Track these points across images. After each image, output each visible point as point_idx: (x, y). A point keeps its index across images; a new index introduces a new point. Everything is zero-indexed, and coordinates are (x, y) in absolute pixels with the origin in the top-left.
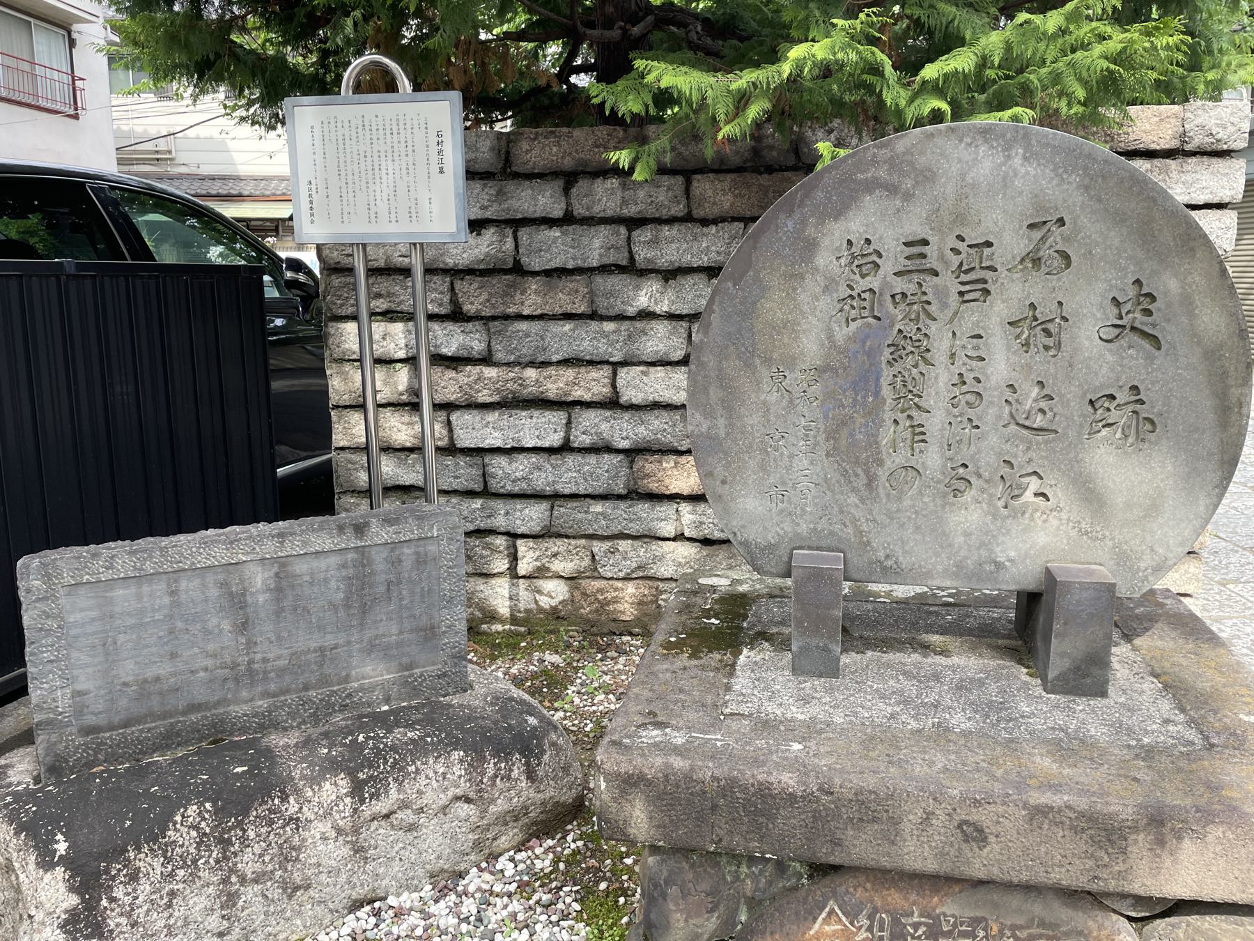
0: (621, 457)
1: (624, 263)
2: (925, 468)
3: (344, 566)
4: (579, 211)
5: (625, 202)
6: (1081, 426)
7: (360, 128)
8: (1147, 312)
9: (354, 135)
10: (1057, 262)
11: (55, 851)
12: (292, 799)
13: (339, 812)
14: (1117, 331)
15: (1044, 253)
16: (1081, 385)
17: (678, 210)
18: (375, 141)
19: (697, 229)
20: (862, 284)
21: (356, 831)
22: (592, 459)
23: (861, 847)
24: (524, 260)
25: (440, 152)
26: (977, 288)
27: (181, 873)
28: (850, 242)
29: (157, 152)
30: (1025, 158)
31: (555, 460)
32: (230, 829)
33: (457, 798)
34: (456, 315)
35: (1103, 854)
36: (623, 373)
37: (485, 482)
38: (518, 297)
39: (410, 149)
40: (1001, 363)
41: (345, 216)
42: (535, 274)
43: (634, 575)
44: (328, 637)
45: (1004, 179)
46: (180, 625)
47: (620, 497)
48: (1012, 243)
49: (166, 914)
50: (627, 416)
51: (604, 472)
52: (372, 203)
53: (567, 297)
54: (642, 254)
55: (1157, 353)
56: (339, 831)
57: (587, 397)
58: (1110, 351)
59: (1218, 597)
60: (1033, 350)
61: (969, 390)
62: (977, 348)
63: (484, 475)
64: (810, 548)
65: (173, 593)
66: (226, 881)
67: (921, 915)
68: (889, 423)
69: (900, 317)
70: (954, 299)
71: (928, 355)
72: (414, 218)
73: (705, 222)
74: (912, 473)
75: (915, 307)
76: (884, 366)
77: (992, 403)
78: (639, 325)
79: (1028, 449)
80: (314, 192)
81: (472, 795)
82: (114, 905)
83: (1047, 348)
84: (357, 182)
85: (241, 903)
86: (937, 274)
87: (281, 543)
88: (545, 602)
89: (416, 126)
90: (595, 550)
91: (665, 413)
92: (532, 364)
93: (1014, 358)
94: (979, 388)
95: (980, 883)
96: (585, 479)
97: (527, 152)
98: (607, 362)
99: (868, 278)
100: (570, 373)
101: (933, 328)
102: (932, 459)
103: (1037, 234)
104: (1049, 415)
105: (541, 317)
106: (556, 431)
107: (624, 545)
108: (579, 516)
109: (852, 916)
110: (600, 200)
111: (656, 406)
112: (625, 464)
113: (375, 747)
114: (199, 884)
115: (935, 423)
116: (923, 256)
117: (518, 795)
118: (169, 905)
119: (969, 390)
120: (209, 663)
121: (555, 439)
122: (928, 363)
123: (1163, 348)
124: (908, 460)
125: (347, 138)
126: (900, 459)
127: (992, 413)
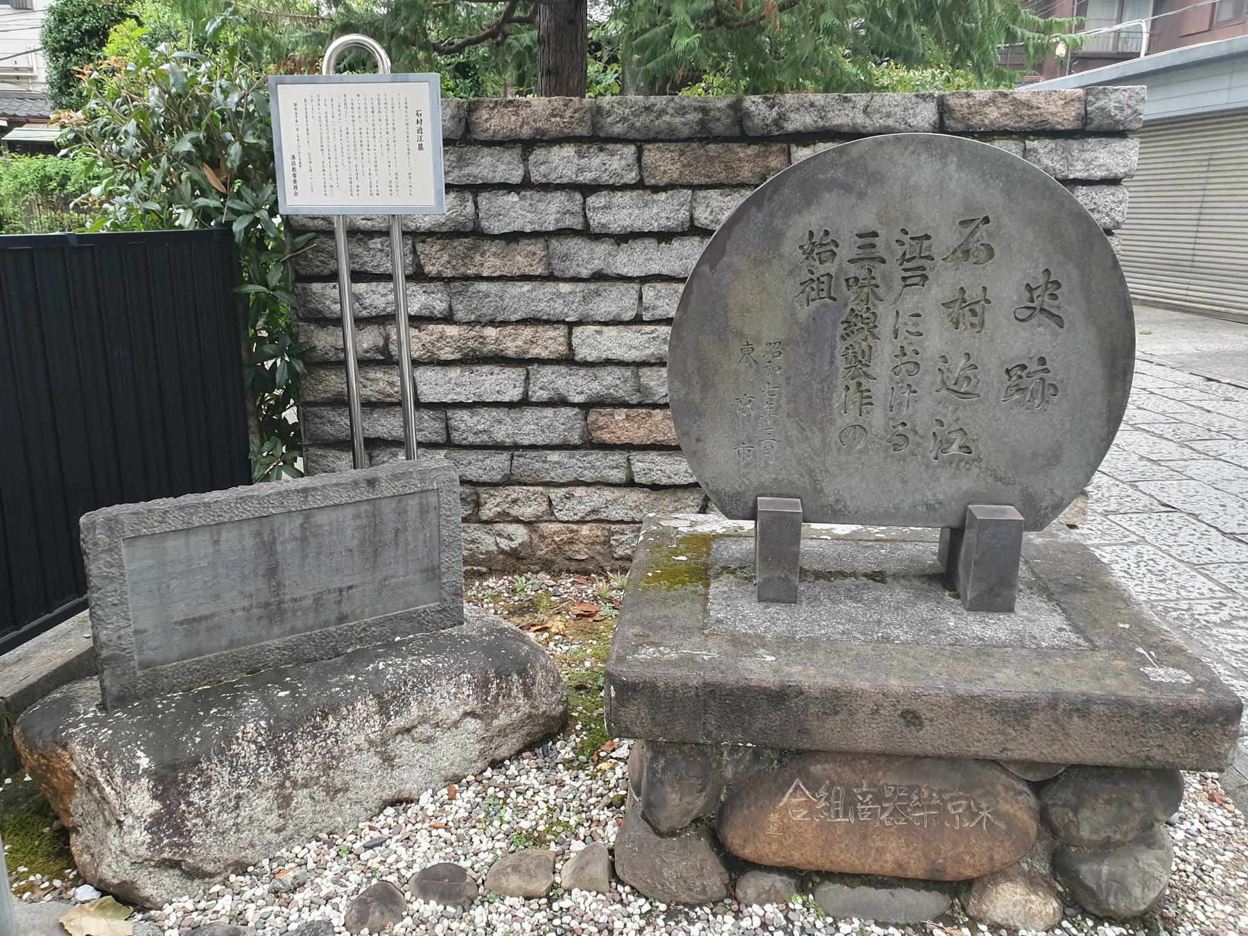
0: (577, 410)
1: (579, 227)
2: (870, 425)
3: (358, 516)
4: (536, 177)
5: (581, 170)
6: (999, 390)
7: (343, 106)
8: (1054, 297)
9: (336, 113)
10: (983, 255)
11: (138, 765)
12: (330, 718)
13: (370, 727)
14: (1029, 312)
15: (972, 246)
16: (999, 357)
17: (631, 177)
18: (356, 118)
19: (648, 196)
20: (821, 269)
21: (384, 743)
22: (549, 412)
23: (828, 732)
24: (485, 224)
25: (420, 131)
26: (916, 274)
27: (245, 779)
28: (811, 234)
29: (17, 69)
30: (959, 166)
31: (514, 413)
32: (283, 742)
33: (466, 714)
34: (418, 276)
35: (1011, 731)
36: (577, 331)
37: (448, 435)
38: (478, 258)
39: (391, 125)
40: (937, 338)
41: (328, 188)
42: (494, 237)
43: (588, 518)
44: (345, 578)
45: (941, 182)
46: (221, 570)
47: (575, 447)
48: (946, 238)
49: (234, 815)
50: (582, 372)
51: (562, 424)
52: (354, 178)
53: (524, 259)
54: (597, 219)
55: (1060, 331)
56: (371, 743)
57: (545, 354)
58: (1024, 328)
59: (1100, 527)
60: (962, 326)
61: (909, 361)
62: (916, 325)
63: (447, 427)
64: (771, 495)
65: (216, 542)
66: (281, 786)
67: (869, 787)
68: (841, 388)
69: (853, 298)
70: (898, 284)
71: (876, 331)
72: (394, 192)
73: (656, 189)
74: (859, 430)
75: (866, 290)
76: (838, 339)
77: (927, 371)
78: (593, 286)
79: (956, 409)
80: (297, 166)
81: (478, 711)
82: (191, 809)
83: (973, 325)
84: (339, 157)
85: (293, 804)
86: (884, 262)
87: (306, 497)
88: (504, 544)
89: (396, 106)
90: (552, 496)
91: (615, 369)
92: (492, 323)
93: (946, 334)
94: (917, 359)
95: (918, 758)
96: (543, 431)
97: (486, 120)
98: (564, 322)
99: (827, 264)
100: (528, 332)
101: (880, 309)
102: (877, 418)
103: (968, 230)
104: (974, 381)
105: (501, 278)
106: (515, 387)
107: (579, 491)
108: (538, 465)
109: (814, 790)
110: (556, 168)
111: (608, 362)
112: (580, 417)
113: (395, 672)
114: (260, 788)
115: (880, 388)
116: (873, 246)
117: (517, 711)
118: (237, 807)
119: (909, 361)
120: (246, 603)
121: (514, 394)
122: (874, 336)
123: (1066, 326)
124: (857, 419)
125: (330, 116)
126: (849, 419)
127: (927, 380)
